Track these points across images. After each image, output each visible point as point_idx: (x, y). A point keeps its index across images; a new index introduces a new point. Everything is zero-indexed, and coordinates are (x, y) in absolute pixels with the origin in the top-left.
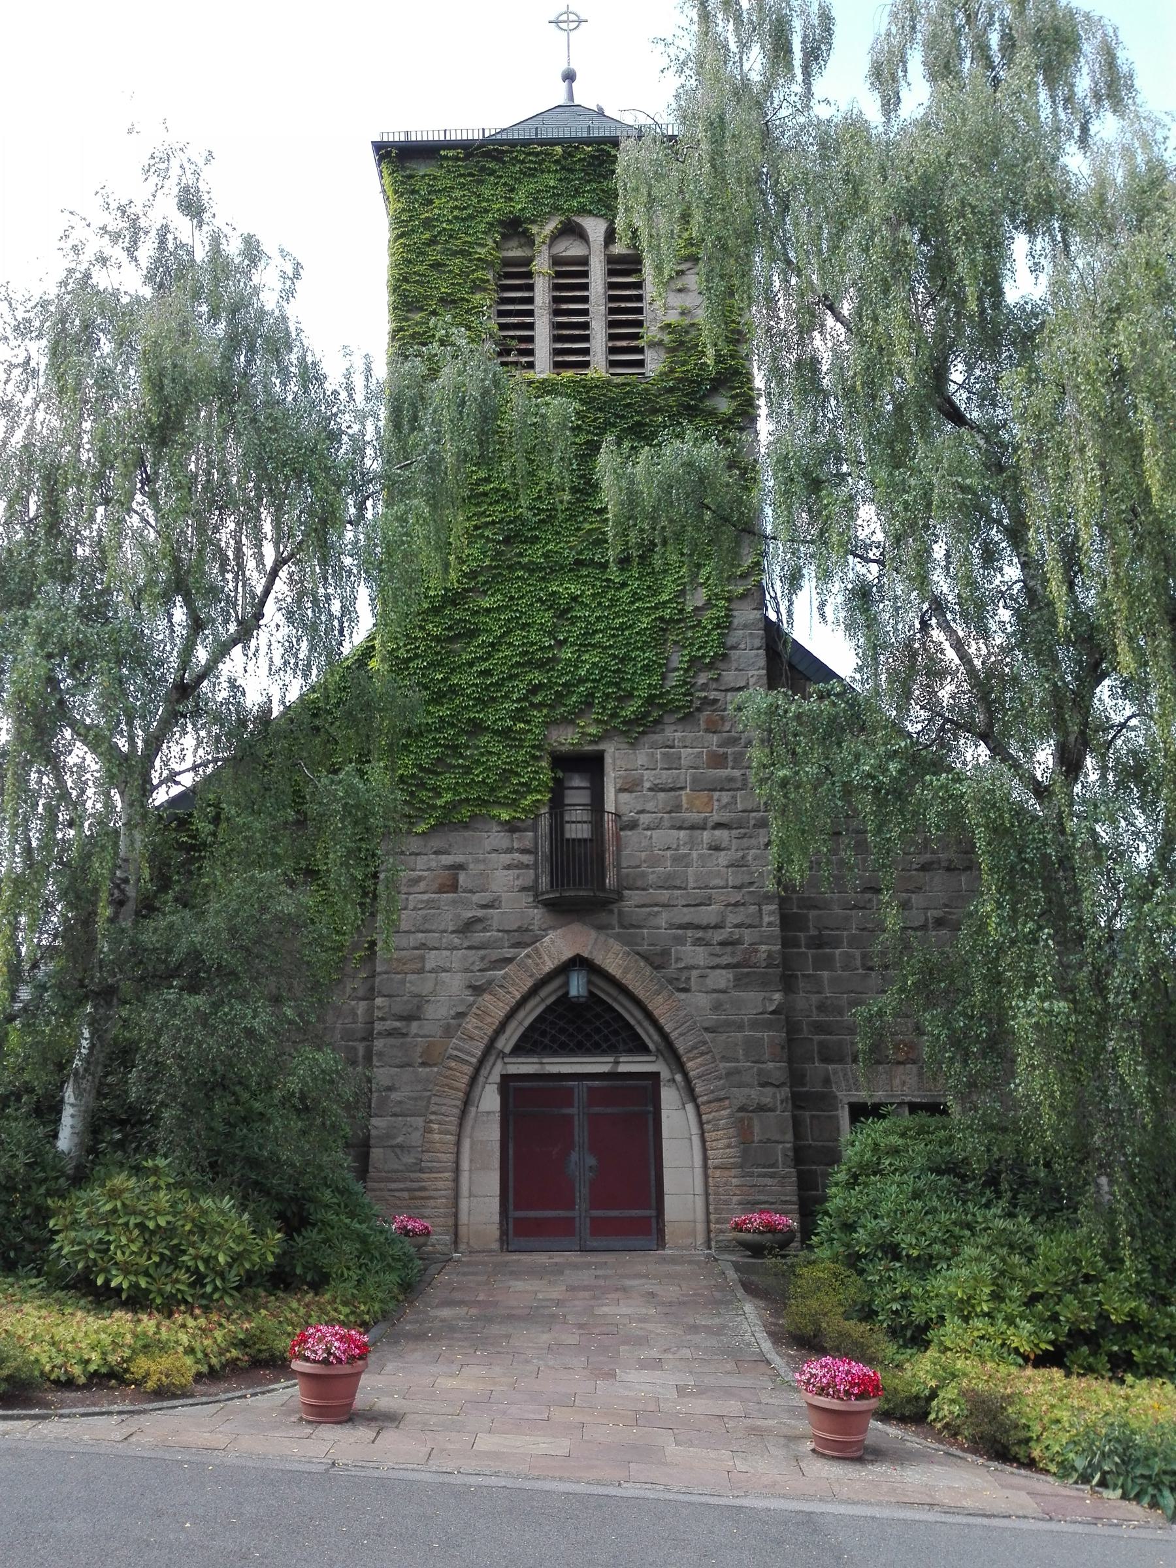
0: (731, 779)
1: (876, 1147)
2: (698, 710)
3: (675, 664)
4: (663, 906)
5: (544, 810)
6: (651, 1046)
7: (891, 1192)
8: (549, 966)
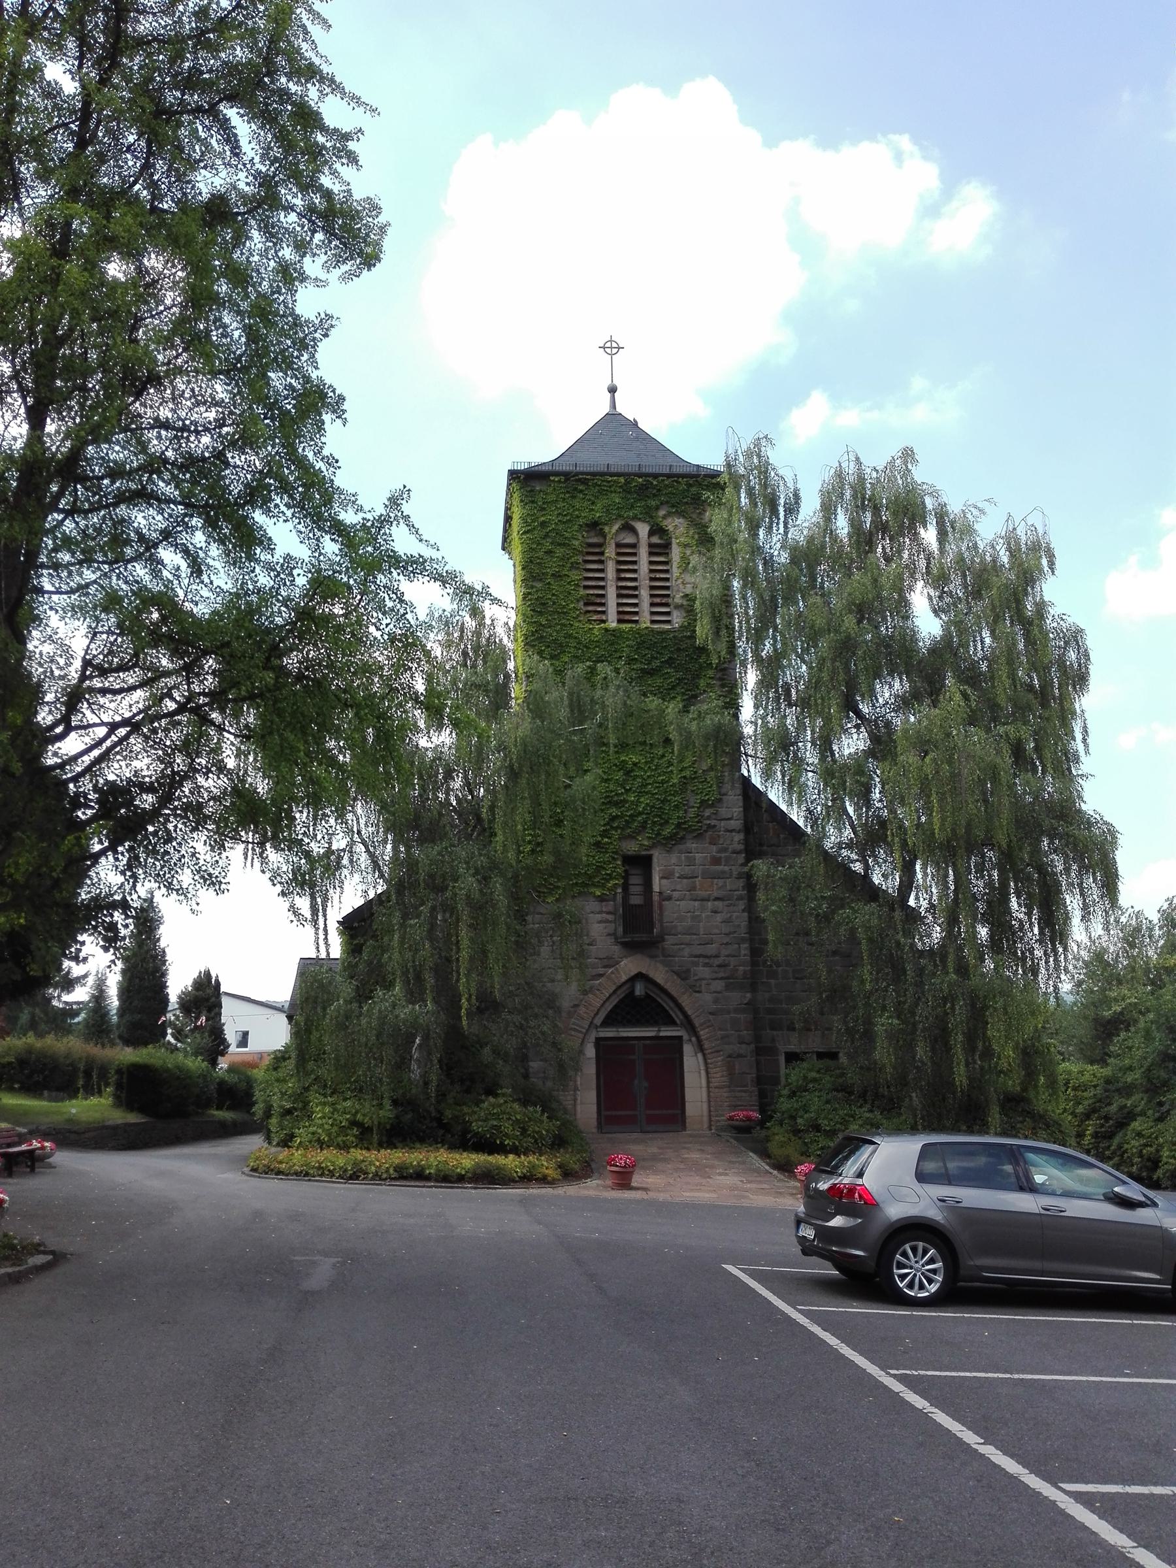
0: (723, 872)
1: (805, 1078)
2: (706, 831)
3: (692, 804)
5: (619, 890)
7: (815, 1101)
8: (624, 978)
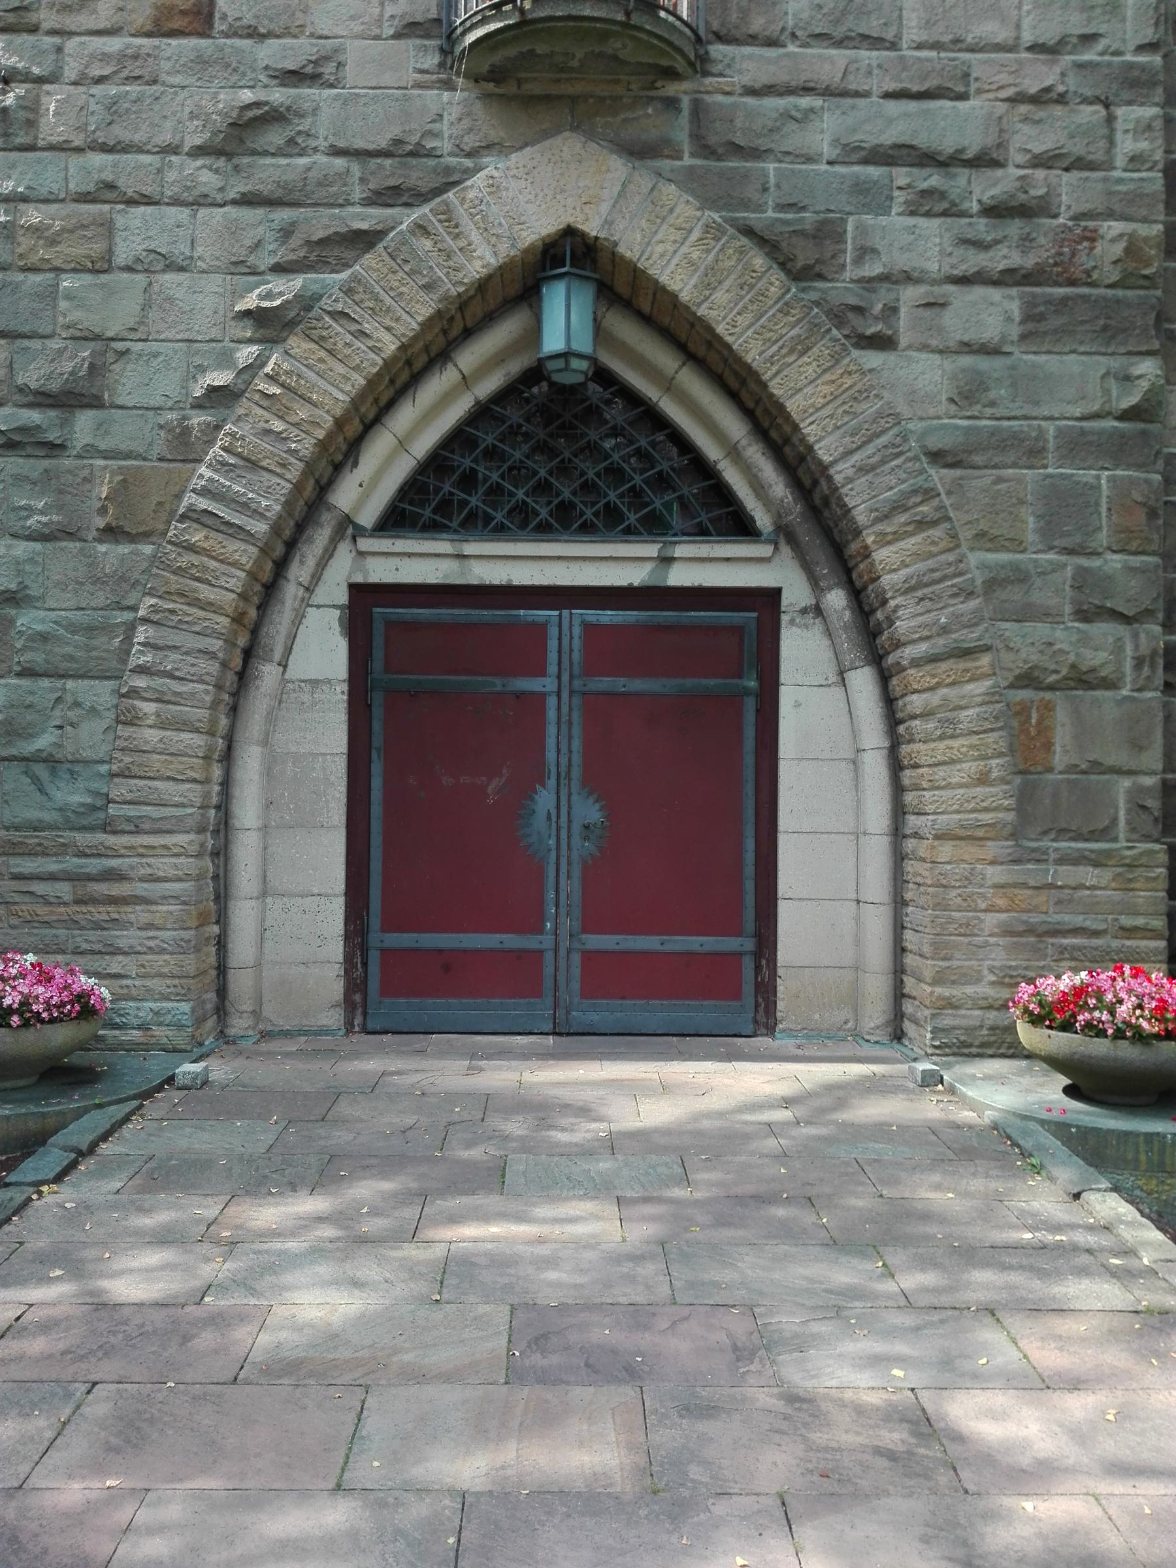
4: (828, 92)
6: (763, 520)
8: (482, 257)
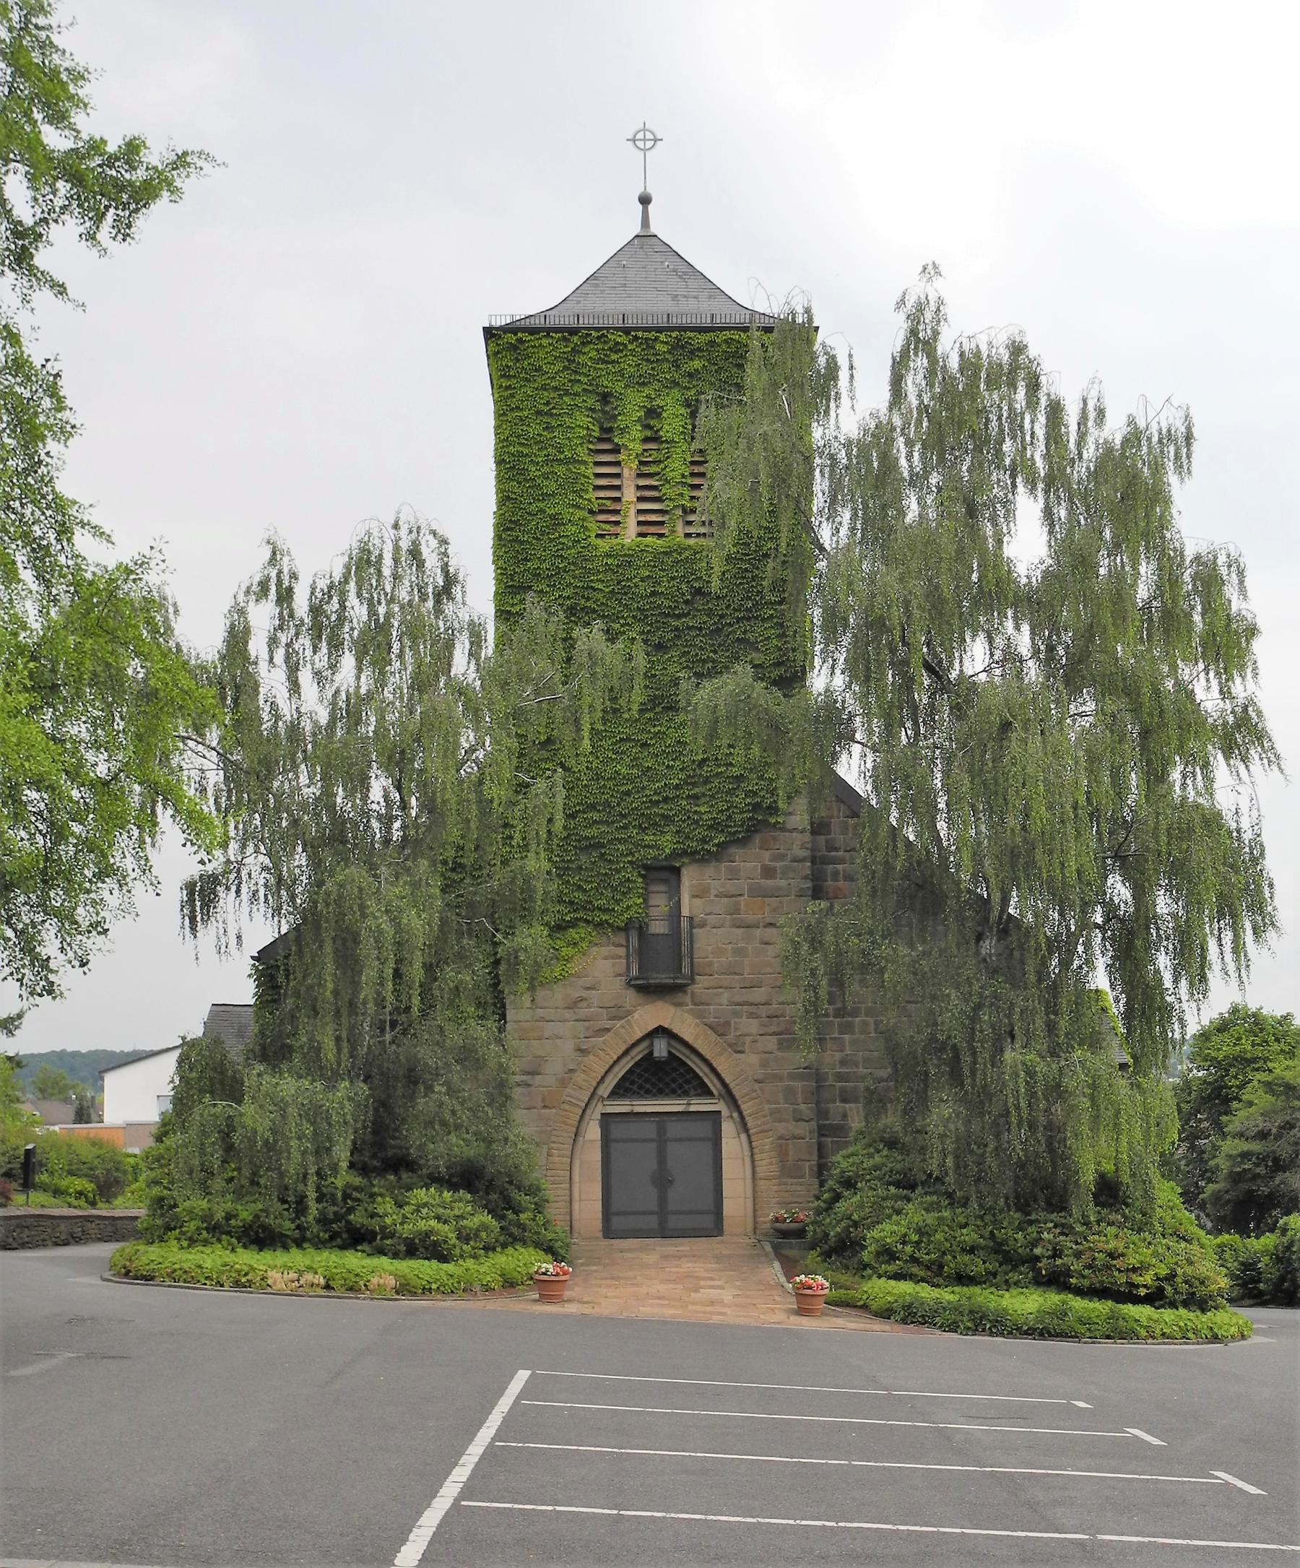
6: (715, 1092)
